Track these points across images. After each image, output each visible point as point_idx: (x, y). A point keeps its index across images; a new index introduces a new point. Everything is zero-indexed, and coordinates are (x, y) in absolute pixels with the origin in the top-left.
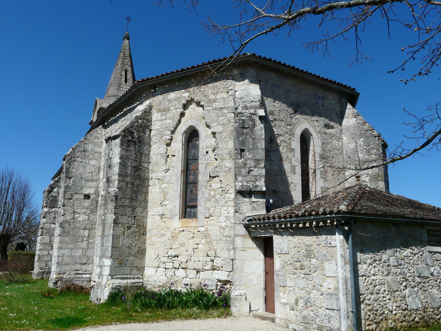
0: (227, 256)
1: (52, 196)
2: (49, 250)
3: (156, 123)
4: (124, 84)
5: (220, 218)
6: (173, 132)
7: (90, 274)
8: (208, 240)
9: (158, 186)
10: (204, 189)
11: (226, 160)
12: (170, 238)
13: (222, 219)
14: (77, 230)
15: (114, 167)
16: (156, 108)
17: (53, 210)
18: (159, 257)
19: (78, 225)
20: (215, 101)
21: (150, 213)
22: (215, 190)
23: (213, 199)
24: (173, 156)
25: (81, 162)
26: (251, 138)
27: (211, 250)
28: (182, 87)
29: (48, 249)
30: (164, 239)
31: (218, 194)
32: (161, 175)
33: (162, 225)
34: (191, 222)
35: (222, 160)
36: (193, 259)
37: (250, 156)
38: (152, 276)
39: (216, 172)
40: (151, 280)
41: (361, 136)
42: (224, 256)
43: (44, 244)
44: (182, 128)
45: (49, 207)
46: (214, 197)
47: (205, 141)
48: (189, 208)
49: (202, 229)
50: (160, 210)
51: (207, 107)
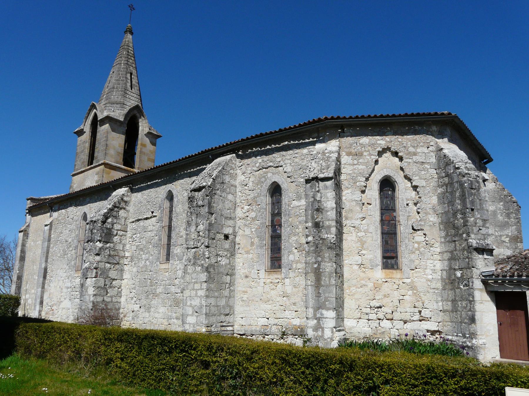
0: (435, 307)
1: (107, 228)
2: (103, 296)
3: (346, 166)
4: (130, 90)
5: (426, 270)
6: (367, 179)
7: (232, 326)
8: (415, 292)
9: (354, 234)
10: (407, 241)
11: (430, 214)
12: (372, 289)
13: (428, 271)
14: (221, 275)
15: (327, 211)
16: (345, 150)
17: (108, 245)
18: (360, 308)
19: (222, 270)
20: (415, 154)
21: (346, 261)
22: (419, 243)
23: (417, 252)
24: (368, 204)
25: (221, 196)
26: (478, 198)
27: (418, 301)
28: (376, 134)
29: (102, 294)
30: (366, 289)
31: (423, 247)
32: (357, 223)
33: (362, 275)
34: (396, 274)
35: (427, 214)
36: (399, 310)
37: (479, 216)
38: (353, 327)
39: (421, 225)
40: (355, 331)
41: (501, 200)
42: (432, 307)
43: (98, 287)
44: (377, 177)
45: (104, 242)
46: (418, 249)
47: (404, 192)
48: (390, 258)
49: (408, 281)
50: (359, 260)
51: (407, 158)
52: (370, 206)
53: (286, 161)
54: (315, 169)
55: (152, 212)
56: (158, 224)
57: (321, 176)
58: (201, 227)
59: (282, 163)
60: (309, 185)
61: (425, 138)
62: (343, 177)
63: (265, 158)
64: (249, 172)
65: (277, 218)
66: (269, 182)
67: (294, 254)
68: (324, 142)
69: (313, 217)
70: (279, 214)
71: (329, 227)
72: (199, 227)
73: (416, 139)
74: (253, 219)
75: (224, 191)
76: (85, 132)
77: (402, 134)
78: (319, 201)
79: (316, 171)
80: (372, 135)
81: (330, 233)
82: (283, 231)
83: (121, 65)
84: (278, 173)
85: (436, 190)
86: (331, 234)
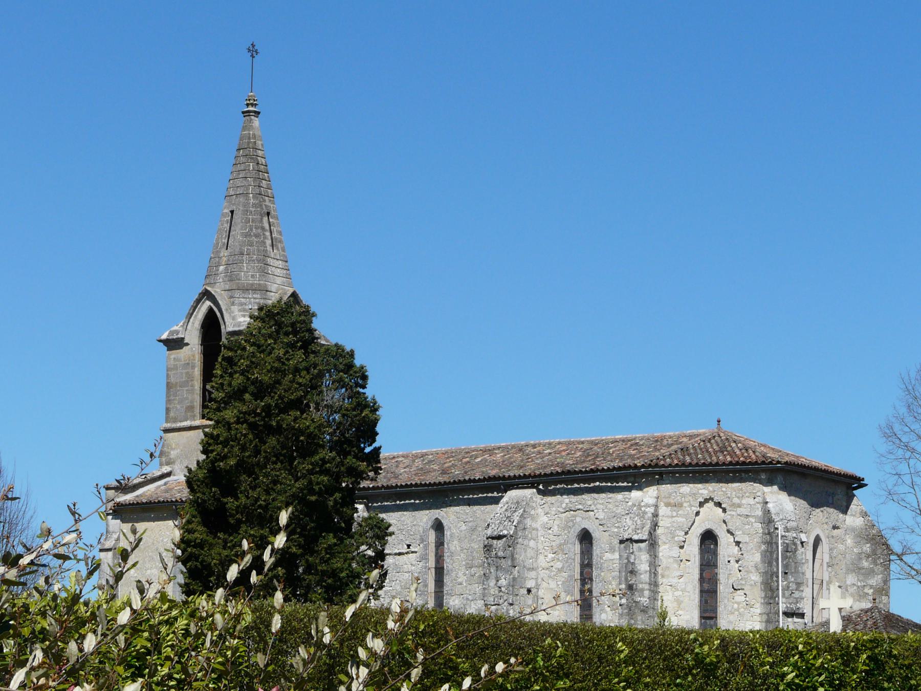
6: (686, 533)
9: (670, 593)
16: (664, 500)
20: (739, 506)
22: (738, 603)
23: (737, 613)
32: (674, 581)
35: (748, 572)
39: (742, 584)
46: (738, 610)
47: (726, 548)
52: (689, 563)
53: (598, 506)
54: (629, 527)
55: (409, 546)
56: (421, 564)
57: (636, 537)
58: (503, 582)
59: (593, 507)
60: (623, 545)
61: (751, 488)
62: (659, 531)
63: (573, 498)
64: (553, 513)
65: (586, 570)
66: (578, 529)
67: (606, 612)
68: (641, 489)
69: (626, 579)
70: (590, 565)
71: (642, 590)
72: (500, 582)
73: (741, 489)
74: (560, 570)
75: (525, 537)
76: (187, 344)
77: (727, 482)
78: (633, 564)
79: (630, 531)
80: (694, 483)
81: (642, 596)
82: (594, 586)
83: (248, 199)
84: (589, 518)
85: (760, 547)
86: (644, 597)
